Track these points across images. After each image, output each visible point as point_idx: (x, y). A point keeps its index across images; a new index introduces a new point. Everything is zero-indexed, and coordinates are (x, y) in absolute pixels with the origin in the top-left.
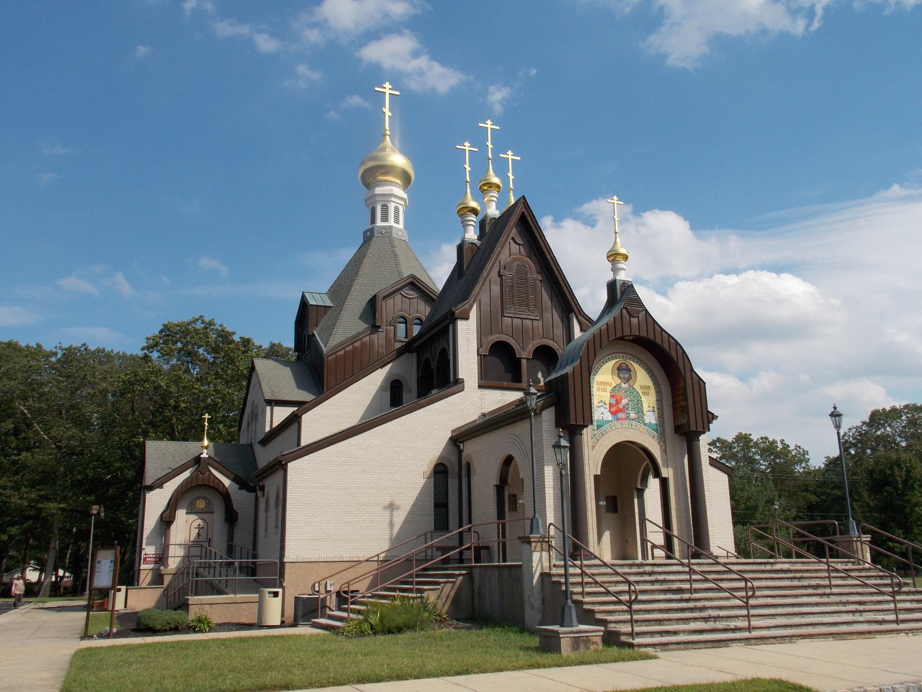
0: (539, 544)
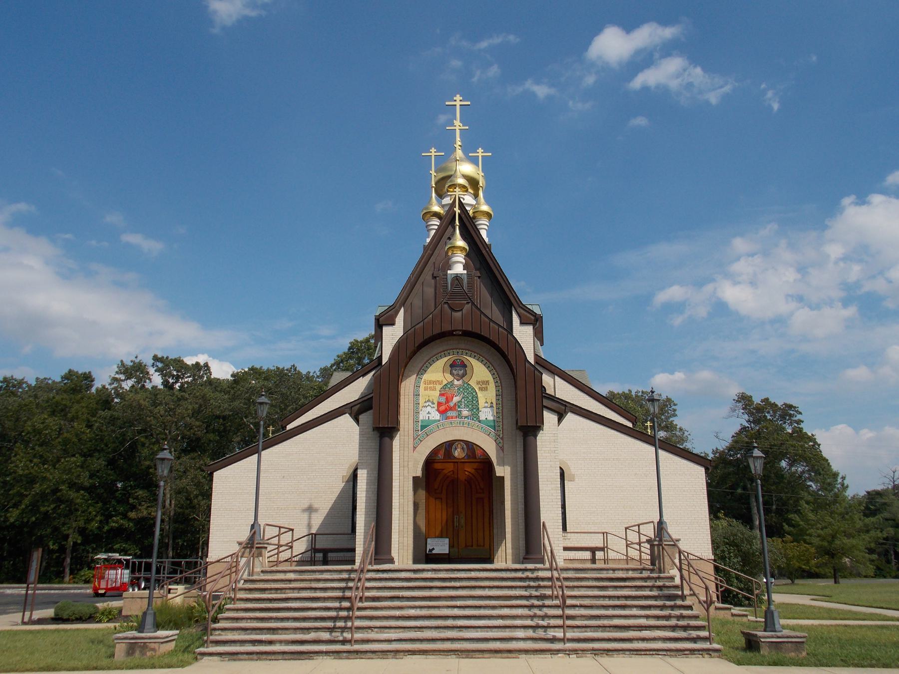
0: (642, 545)
